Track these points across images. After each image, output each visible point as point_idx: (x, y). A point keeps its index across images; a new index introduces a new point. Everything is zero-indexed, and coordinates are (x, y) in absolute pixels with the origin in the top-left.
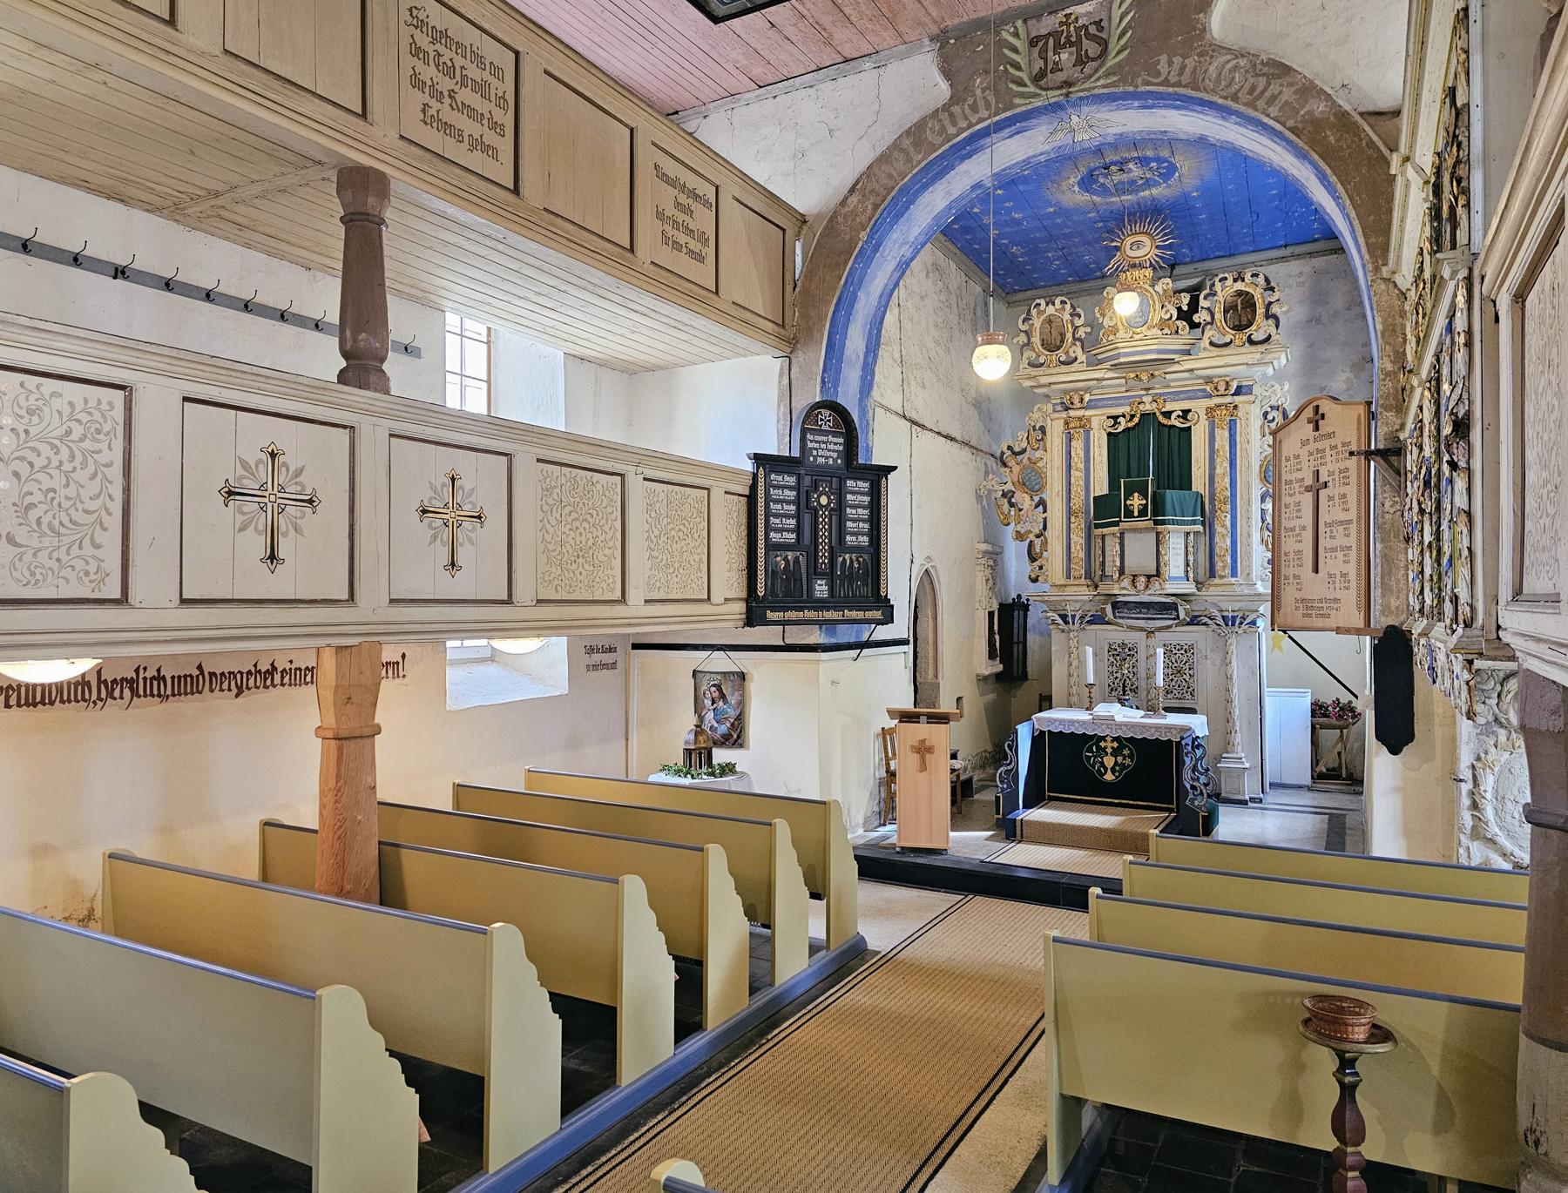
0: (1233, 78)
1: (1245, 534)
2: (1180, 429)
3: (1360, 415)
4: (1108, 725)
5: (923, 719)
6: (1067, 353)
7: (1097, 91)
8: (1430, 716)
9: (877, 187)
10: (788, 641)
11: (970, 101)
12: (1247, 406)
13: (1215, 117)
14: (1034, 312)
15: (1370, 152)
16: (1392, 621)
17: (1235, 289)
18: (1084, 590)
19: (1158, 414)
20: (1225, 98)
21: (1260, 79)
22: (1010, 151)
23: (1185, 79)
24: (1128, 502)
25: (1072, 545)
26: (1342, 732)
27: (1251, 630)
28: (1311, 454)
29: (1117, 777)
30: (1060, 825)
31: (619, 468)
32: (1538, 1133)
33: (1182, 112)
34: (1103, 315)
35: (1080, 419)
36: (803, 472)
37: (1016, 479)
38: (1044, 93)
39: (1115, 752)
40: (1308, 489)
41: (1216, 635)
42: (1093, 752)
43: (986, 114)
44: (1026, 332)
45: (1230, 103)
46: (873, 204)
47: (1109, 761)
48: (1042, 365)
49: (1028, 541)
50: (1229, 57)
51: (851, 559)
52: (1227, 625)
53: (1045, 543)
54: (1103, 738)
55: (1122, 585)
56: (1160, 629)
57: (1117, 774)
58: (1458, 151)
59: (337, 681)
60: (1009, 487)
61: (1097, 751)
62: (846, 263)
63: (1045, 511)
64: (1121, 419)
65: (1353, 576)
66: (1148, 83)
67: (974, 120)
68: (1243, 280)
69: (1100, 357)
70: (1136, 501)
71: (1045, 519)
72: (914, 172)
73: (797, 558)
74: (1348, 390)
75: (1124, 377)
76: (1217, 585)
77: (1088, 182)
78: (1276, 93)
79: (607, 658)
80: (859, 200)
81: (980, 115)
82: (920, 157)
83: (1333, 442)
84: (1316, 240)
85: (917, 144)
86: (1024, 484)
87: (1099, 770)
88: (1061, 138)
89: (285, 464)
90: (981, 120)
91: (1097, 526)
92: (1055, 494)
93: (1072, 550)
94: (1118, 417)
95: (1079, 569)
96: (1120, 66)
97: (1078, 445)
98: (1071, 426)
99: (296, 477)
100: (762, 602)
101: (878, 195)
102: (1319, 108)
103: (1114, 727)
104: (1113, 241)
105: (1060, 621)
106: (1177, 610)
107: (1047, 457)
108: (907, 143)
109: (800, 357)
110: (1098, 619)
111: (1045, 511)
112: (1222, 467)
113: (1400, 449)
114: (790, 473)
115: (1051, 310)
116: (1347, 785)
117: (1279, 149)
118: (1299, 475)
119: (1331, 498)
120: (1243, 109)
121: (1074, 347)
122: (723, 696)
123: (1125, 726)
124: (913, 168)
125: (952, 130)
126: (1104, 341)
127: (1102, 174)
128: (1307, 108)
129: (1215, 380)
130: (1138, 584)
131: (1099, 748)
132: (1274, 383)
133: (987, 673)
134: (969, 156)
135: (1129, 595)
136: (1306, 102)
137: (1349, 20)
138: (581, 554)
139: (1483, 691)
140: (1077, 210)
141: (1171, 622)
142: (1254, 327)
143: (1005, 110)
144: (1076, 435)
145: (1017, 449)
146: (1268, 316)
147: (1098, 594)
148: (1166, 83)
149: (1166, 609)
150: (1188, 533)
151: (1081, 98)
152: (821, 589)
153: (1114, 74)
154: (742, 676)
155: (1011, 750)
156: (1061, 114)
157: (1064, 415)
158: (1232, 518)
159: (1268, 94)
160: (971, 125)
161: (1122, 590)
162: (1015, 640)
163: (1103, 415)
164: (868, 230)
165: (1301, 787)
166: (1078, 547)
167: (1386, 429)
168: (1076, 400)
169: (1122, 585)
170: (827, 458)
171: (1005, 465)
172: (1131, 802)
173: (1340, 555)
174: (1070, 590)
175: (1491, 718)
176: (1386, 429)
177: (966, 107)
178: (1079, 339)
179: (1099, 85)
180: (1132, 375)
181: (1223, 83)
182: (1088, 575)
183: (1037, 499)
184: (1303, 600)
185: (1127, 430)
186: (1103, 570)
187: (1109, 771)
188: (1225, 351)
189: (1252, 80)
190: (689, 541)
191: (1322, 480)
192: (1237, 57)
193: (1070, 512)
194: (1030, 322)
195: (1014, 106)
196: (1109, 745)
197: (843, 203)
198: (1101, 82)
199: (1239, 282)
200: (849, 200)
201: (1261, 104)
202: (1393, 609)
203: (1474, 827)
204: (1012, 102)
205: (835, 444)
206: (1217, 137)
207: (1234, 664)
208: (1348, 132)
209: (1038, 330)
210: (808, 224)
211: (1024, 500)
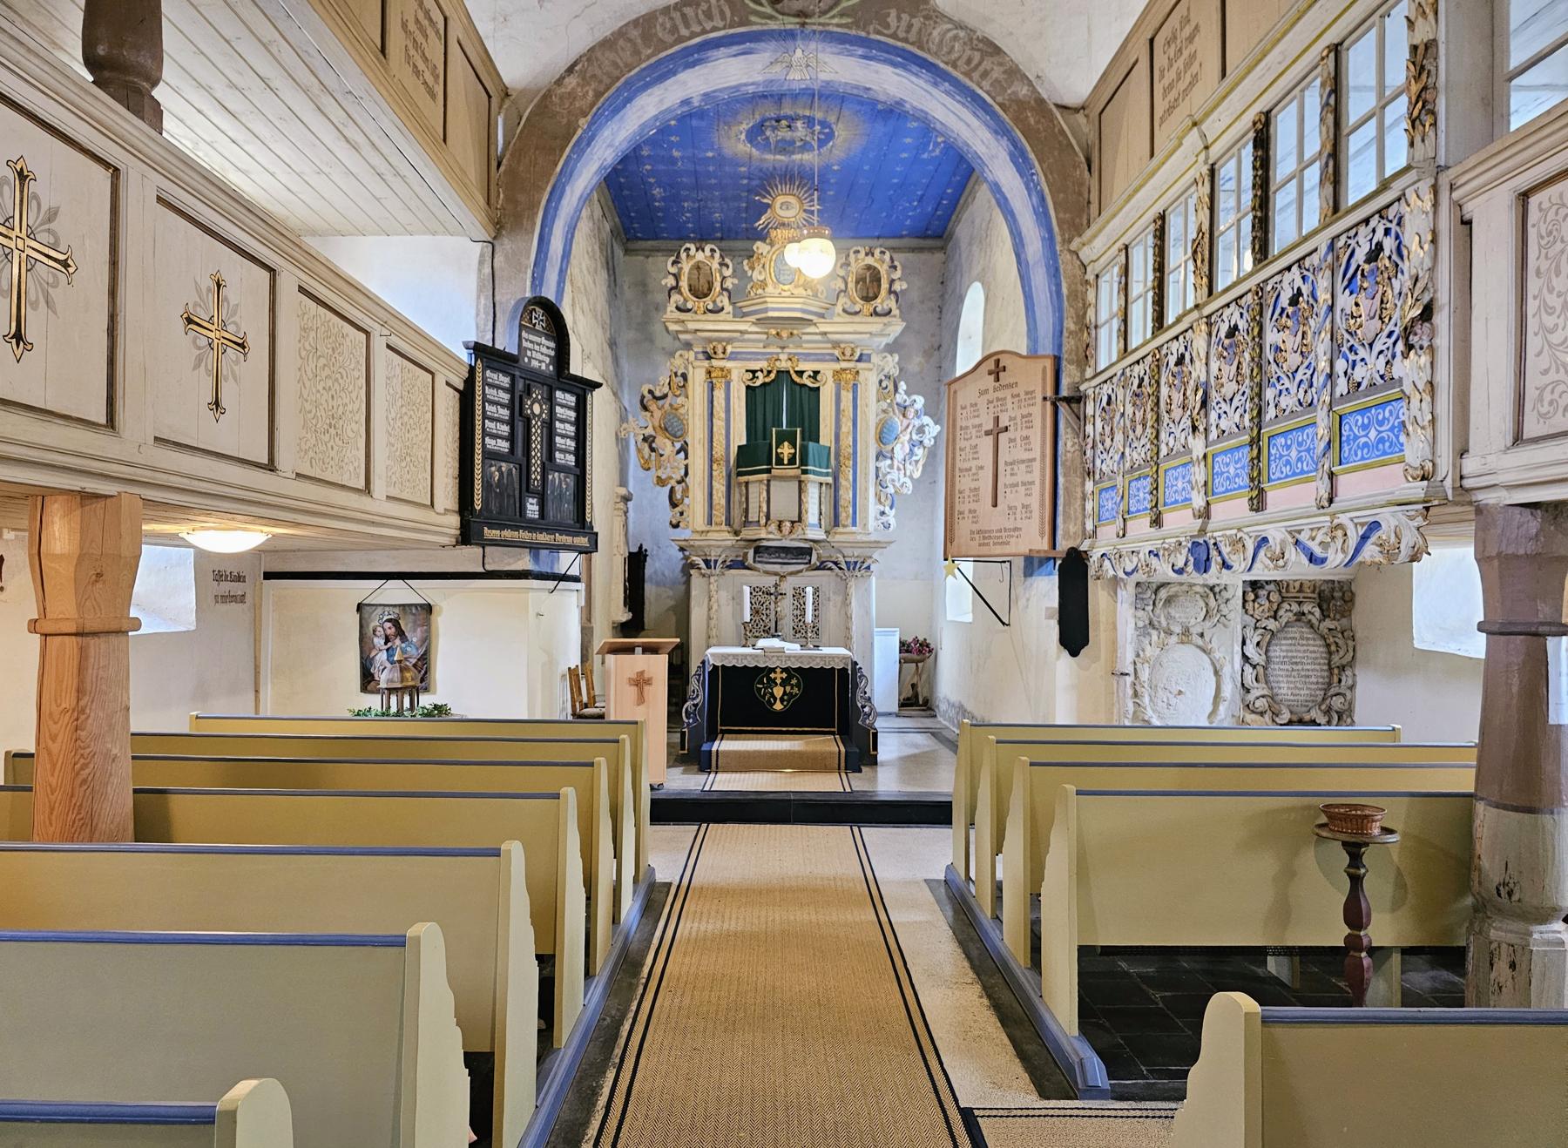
0: (953, 47)
2: (810, 388)
3: (1045, 368)
5: (639, 650)
6: (714, 302)
7: (831, 28)
8: (1097, 622)
9: (598, 72)
10: (489, 568)
11: (704, 6)
12: (866, 372)
13: (926, 81)
14: (683, 255)
15: (1061, 138)
16: (1071, 544)
17: (866, 262)
18: (726, 536)
19: (792, 372)
20: (947, 63)
21: (976, 53)
22: (691, 85)
23: (912, 36)
24: (779, 450)
25: (714, 492)
28: (990, 402)
30: (755, 752)
31: (366, 322)
32: (1511, 885)
33: (897, 71)
34: (753, 269)
35: (722, 369)
36: (517, 373)
37: (657, 424)
38: (781, 17)
39: (784, 683)
40: (988, 433)
41: (839, 580)
42: (763, 684)
43: (721, 24)
44: (674, 275)
45: (950, 69)
46: (595, 90)
48: (689, 310)
49: (669, 486)
50: (950, 26)
51: (560, 478)
52: (849, 569)
53: (686, 491)
54: (773, 670)
55: (770, 529)
56: (792, 574)
58: (1428, 78)
59: (82, 549)
60: (650, 431)
62: (562, 150)
63: (686, 458)
64: (759, 374)
65: (1035, 506)
66: (879, 33)
67: (708, 26)
68: (873, 255)
69: (745, 310)
70: (786, 450)
71: (686, 467)
72: (643, 66)
73: (511, 470)
74: (921, 372)
75: (767, 333)
76: (841, 533)
77: (756, 134)
78: (988, 68)
79: (236, 589)
80: (578, 84)
81: (715, 24)
82: (649, 51)
83: (1015, 391)
84: (902, 237)
85: (647, 37)
86: (666, 430)
88: (777, 71)
89: (36, 197)
90: (714, 29)
91: (740, 474)
92: (696, 441)
93: (714, 497)
95: (719, 515)
96: (853, 10)
97: (719, 395)
98: (713, 375)
99: (49, 221)
100: (478, 517)
101: (601, 82)
102: (1023, 91)
103: (784, 659)
104: (765, 197)
105: (703, 565)
107: (688, 404)
108: (635, 34)
109: (506, 245)
110: (740, 565)
111: (686, 458)
112: (846, 427)
113: (1081, 397)
114: (505, 373)
115: (700, 256)
116: (923, 710)
117: (975, 122)
118: (977, 421)
119: (1011, 441)
120: (961, 77)
121: (721, 297)
122: (401, 633)
123: (794, 657)
124: (641, 61)
125: (684, 32)
126: (752, 294)
127: (772, 126)
128: (1013, 89)
129: (842, 346)
130: (783, 529)
131: (769, 679)
133: (624, 620)
134: (693, 65)
136: (1012, 82)
137: (1042, 20)
138: (333, 423)
139: (1143, 599)
140: (735, 162)
141: (802, 567)
142: (879, 300)
143: (741, 24)
144: (718, 385)
145: (658, 394)
146: (890, 292)
147: (741, 540)
148: (894, 36)
149: (803, 553)
150: (821, 484)
151: (814, 32)
152: (532, 508)
153: (848, 16)
154: (428, 609)
156: (790, 44)
159: (981, 69)
160: (704, 32)
161: (770, 536)
163: (741, 368)
164: (589, 117)
165: (890, 714)
166: (720, 495)
167: (1068, 380)
168: (720, 350)
169: (770, 529)
170: (540, 362)
171: (645, 408)
173: (1022, 489)
174: (711, 536)
175: (1147, 622)
176: (1068, 380)
177: (700, 12)
178: (726, 290)
179: (834, 23)
180: (774, 332)
181: (945, 49)
182: (728, 522)
183: (678, 445)
184: (979, 532)
185: (764, 385)
186: (746, 517)
187: (778, 701)
188: (857, 319)
189: (968, 52)
190: (417, 432)
191: (1002, 425)
192: (956, 28)
193: (711, 460)
194: (679, 265)
195: (749, 23)
196: (778, 676)
197: (559, 82)
198: (835, 21)
199: (870, 256)
200: (567, 80)
201: (976, 75)
202: (1071, 533)
203: (1135, 712)
204: (747, 19)
205: (548, 348)
206: (915, 104)
207: (853, 604)
208: (1044, 117)
209: (686, 275)
210: (512, 98)
211: (666, 446)
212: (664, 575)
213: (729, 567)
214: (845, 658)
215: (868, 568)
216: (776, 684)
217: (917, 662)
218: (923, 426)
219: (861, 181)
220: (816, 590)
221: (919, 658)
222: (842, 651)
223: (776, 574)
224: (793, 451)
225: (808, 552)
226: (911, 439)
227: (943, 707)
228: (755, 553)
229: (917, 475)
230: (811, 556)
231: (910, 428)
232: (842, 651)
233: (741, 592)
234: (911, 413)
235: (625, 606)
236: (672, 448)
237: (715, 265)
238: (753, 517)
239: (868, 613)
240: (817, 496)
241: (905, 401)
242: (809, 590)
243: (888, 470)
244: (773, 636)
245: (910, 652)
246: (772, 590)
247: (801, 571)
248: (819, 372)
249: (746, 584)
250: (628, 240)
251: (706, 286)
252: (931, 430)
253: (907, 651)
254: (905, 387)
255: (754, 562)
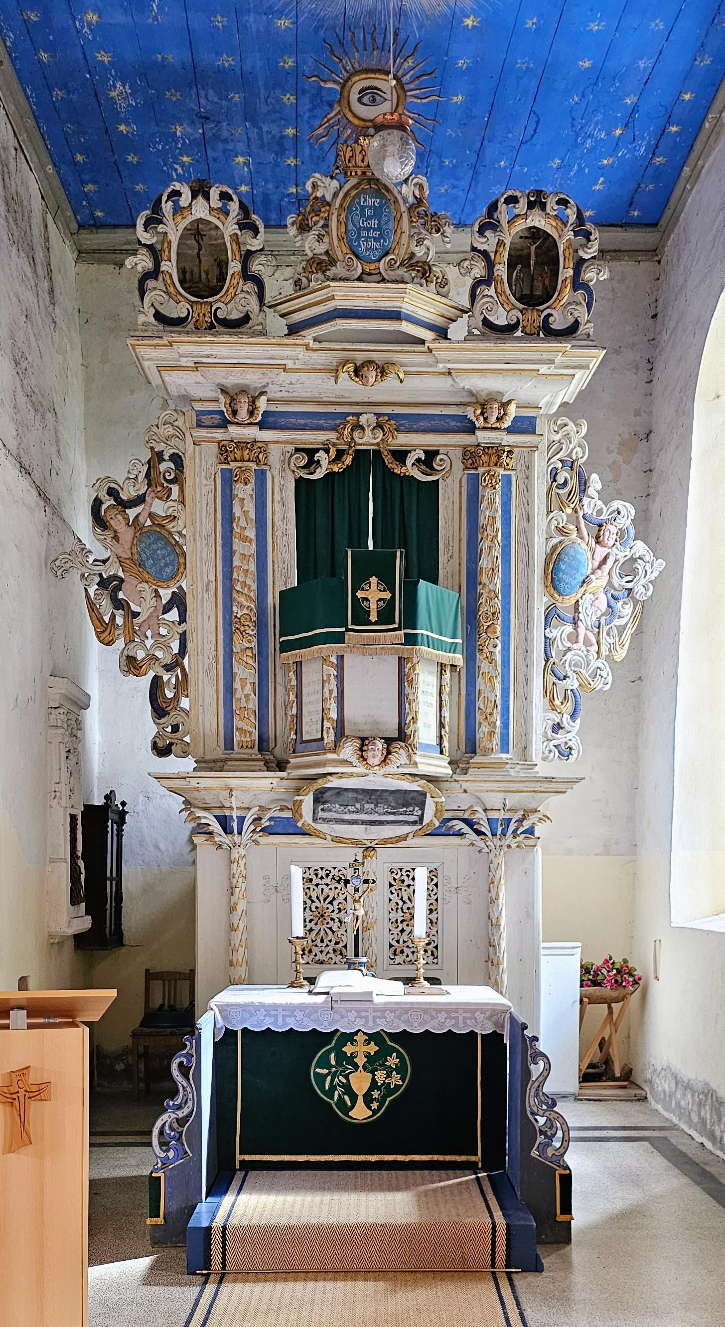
1: (521, 678)
4: (359, 1011)
14: (167, 207)
17: (530, 223)
24: (360, 594)
25: (237, 685)
26: (610, 1008)
27: (528, 842)
29: (375, 1112)
39: (373, 1063)
42: (330, 1066)
44: (150, 248)
47: (360, 1082)
49: (151, 674)
52: (494, 835)
53: (182, 685)
54: (349, 1038)
56: (386, 841)
57: (375, 1105)
60: (113, 569)
61: (339, 1063)
63: (183, 619)
64: (321, 455)
68: (543, 207)
71: (183, 638)
87: (341, 1100)
94: (317, 450)
97: (244, 492)
105: (216, 827)
106: (422, 806)
111: (183, 619)
115: (200, 210)
123: (393, 1011)
131: (342, 1057)
132: (566, 420)
135: (351, 775)
150: (442, 666)
155: (186, 1076)
157: (219, 434)
158: (503, 649)
162: (109, 875)
166: (248, 689)
172: (400, 1158)
183: (166, 594)
185: (330, 476)
187: (360, 1100)
196: (360, 1050)
199: (536, 211)
207: (502, 900)
212: (157, 848)
213: (268, 831)
214: (495, 1012)
215: (530, 831)
216: (356, 1067)
217: (609, 1002)
218: (633, 560)
219: (520, 64)
220: (433, 874)
221: (614, 994)
222: (482, 995)
223: (357, 843)
224: (387, 595)
225: (417, 800)
226: (610, 583)
227: (663, 1085)
228: (317, 800)
229: (620, 654)
230: (423, 809)
231: (610, 562)
232: (482, 995)
233: (288, 877)
234: (610, 533)
235: (74, 901)
236: (153, 602)
237: (229, 228)
238: (310, 731)
239: (529, 914)
240: (434, 691)
241: (600, 512)
242: (422, 875)
243: (569, 644)
244: (350, 965)
245: (600, 985)
246: (349, 874)
247: (405, 838)
248: (437, 453)
249: (297, 863)
250: (81, 226)
251: (216, 271)
252: (648, 568)
253: (595, 983)
254: (599, 486)
255: (315, 820)
